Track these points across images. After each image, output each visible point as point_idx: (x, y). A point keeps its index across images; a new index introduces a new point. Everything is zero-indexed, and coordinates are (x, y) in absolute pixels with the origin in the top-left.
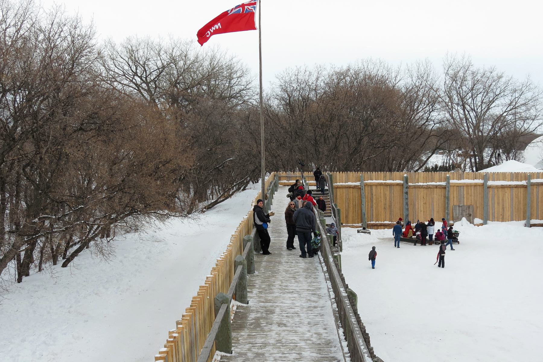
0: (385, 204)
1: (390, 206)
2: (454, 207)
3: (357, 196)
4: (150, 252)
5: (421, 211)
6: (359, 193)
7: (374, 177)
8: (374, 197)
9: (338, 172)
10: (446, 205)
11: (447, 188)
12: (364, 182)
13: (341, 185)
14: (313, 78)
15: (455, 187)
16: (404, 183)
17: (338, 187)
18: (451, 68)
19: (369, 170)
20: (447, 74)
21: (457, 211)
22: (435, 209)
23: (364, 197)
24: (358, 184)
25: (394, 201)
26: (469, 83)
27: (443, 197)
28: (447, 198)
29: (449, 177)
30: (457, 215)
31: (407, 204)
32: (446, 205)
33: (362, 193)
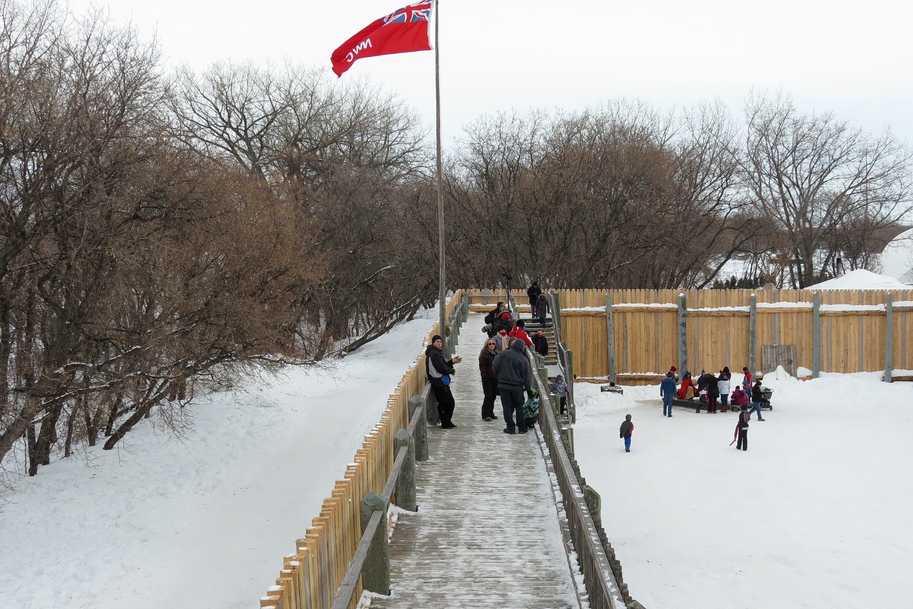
0: (648, 344)
1: (656, 347)
2: (763, 348)
3: (600, 329)
4: (252, 424)
5: (708, 355)
6: (604, 325)
7: (629, 299)
8: (629, 332)
9: (568, 290)
10: (750, 345)
11: (752, 317)
12: (612, 306)
13: (574, 311)
14: (527, 132)
15: (765, 315)
16: (680, 309)
17: (568, 315)
18: (759, 114)
19: (620, 286)
20: (751, 124)
21: (769, 355)
22: (731, 352)
23: (612, 331)
24: (602, 309)
25: (662, 338)
26: (789, 140)
27: (744, 332)
28: (751, 334)
29: (755, 297)
30: (769, 362)
31: (684, 343)
32: (750, 345)
33: (608, 325)
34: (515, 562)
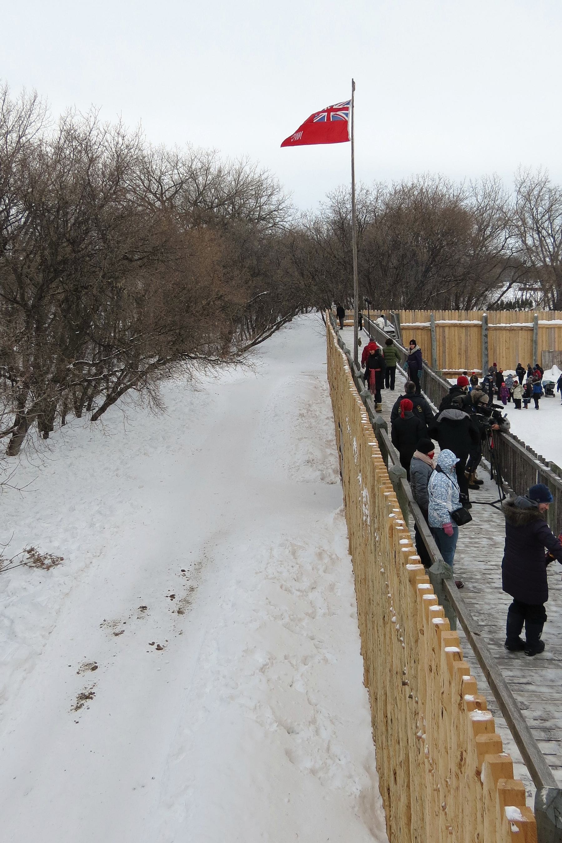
0: (460, 349)
1: (466, 351)
2: (543, 352)
3: (426, 339)
4: (192, 404)
5: (503, 357)
6: (429, 335)
7: (447, 317)
8: (447, 340)
9: (404, 311)
10: (534, 350)
11: (535, 331)
12: (435, 322)
13: (408, 326)
14: (372, 198)
15: (544, 329)
16: (483, 325)
17: (405, 328)
18: (524, 185)
19: (438, 308)
20: (519, 192)
21: (547, 357)
22: (520, 355)
23: (435, 340)
24: (427, 324)
25: (470, 345)
26: (546, 203)
27: (529, 341)
28: (534, 342)
29: (537, 316)
30: (547, 362)
31: (486, 349)
32: (534, 350)
33: (432, 336)
34: (483, 513)
